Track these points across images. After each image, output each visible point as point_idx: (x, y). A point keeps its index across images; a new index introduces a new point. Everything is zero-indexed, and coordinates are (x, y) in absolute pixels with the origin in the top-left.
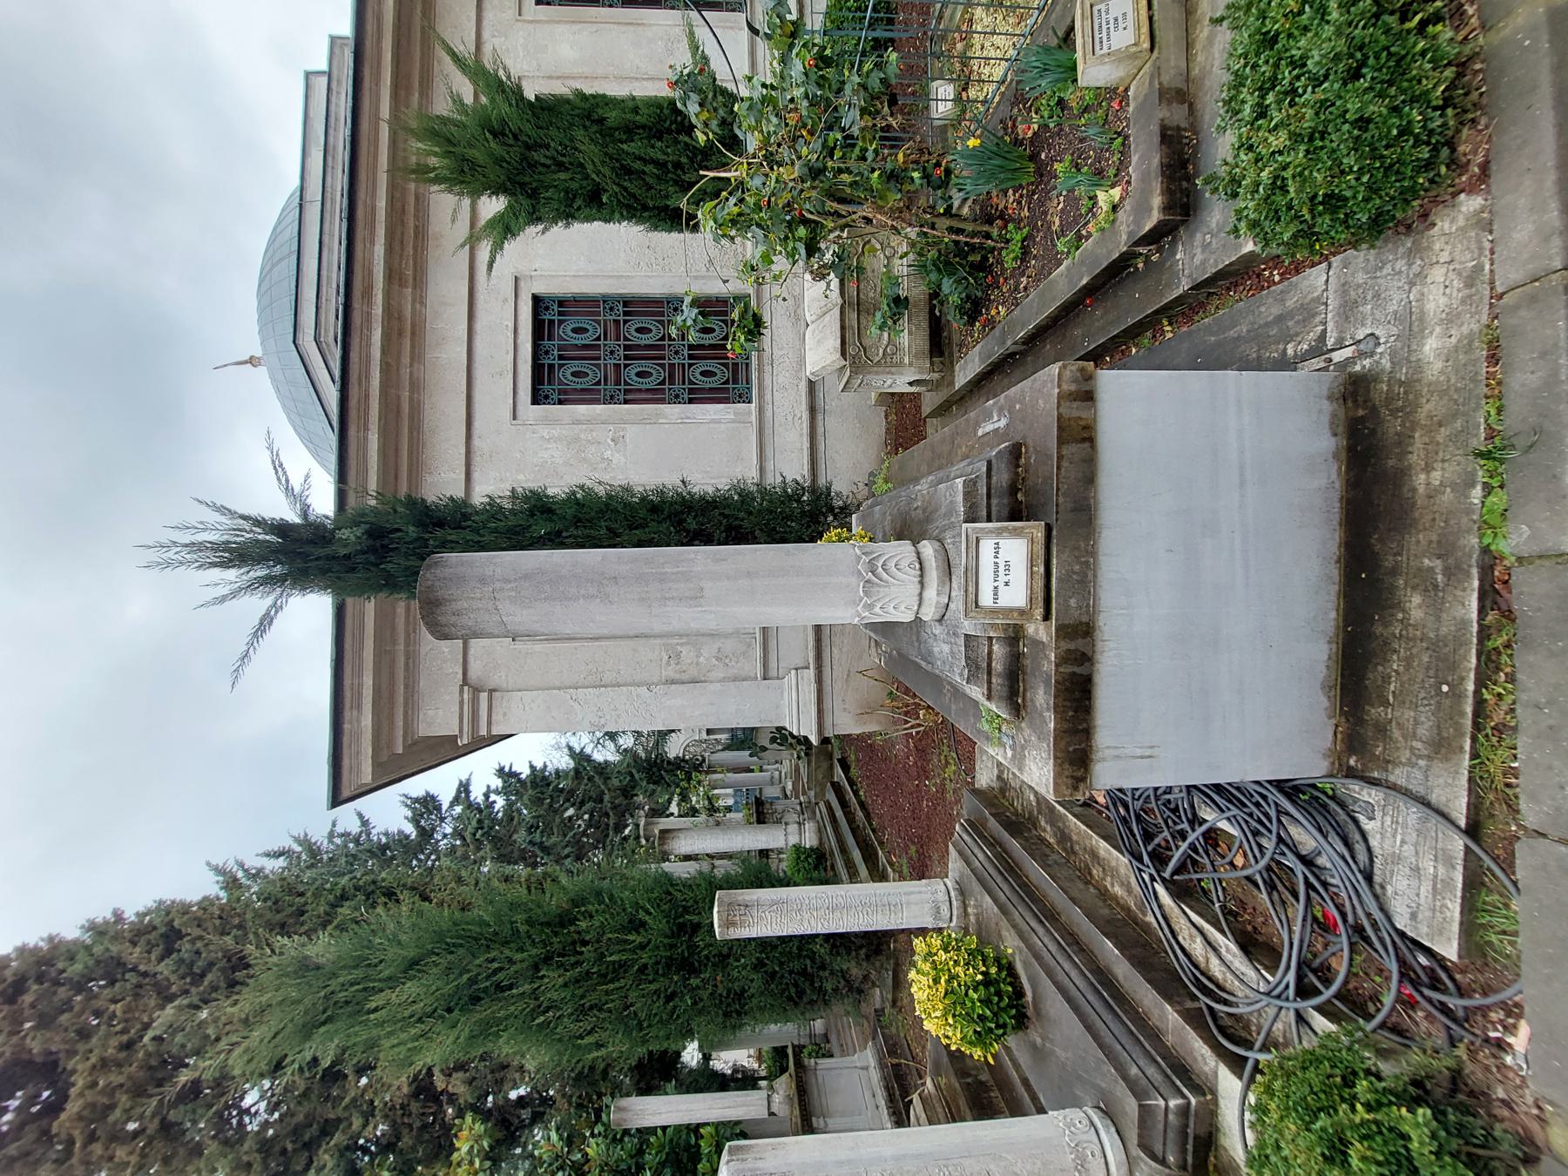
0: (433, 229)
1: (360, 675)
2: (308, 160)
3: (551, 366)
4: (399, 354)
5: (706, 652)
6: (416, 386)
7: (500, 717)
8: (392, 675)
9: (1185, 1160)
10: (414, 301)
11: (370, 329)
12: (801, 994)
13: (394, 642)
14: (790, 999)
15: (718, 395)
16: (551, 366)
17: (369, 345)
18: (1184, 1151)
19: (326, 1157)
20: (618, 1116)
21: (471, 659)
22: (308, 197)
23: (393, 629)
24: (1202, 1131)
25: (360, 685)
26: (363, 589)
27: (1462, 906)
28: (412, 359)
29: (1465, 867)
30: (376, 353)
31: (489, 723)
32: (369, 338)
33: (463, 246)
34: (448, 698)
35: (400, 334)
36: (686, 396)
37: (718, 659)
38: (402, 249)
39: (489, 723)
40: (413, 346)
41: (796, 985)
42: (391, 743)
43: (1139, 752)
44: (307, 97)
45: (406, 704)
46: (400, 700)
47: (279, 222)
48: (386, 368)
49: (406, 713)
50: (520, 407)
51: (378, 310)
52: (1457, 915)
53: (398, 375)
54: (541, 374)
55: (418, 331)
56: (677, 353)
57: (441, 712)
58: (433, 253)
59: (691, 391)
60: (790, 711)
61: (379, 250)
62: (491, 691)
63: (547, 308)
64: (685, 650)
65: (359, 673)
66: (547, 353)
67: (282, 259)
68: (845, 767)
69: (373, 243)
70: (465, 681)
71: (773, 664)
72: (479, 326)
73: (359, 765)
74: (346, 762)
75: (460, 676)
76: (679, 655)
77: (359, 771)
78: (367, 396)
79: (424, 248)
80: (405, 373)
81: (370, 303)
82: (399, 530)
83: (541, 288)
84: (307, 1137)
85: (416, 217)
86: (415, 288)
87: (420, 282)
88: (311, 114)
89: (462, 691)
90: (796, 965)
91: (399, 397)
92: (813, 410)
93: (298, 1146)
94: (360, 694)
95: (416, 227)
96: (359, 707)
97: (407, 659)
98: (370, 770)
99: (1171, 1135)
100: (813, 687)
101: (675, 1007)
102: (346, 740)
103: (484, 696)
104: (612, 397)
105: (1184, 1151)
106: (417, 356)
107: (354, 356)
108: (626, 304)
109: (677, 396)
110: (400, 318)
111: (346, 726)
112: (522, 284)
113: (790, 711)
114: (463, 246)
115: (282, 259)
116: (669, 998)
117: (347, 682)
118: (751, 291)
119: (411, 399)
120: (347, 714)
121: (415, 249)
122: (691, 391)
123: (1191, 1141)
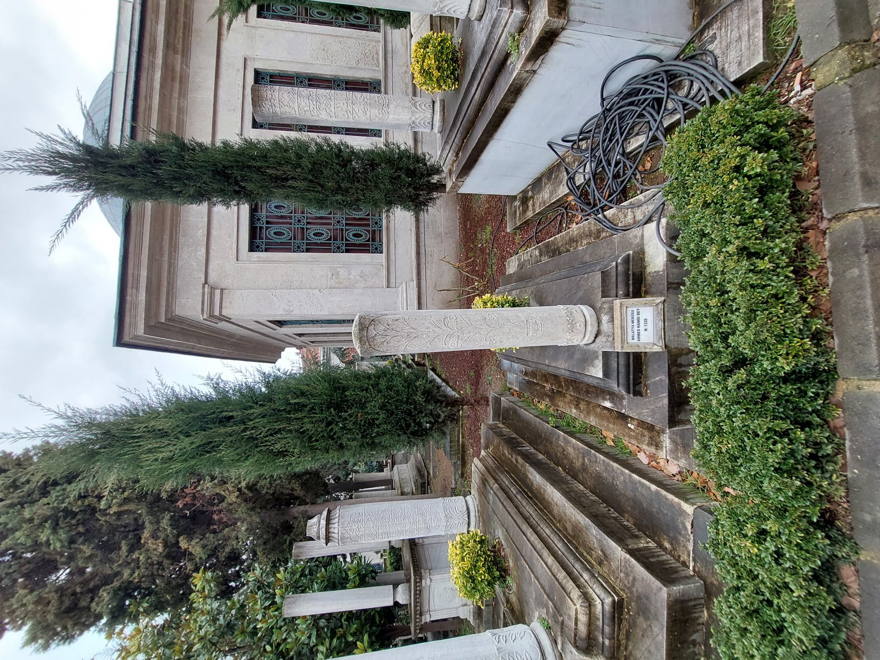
0: (196, 25)
1: (139, 269)
2: (119, 49)
3: (261, 228)
4: (172, 90)
5: (354, 272)
6: (181, 111)
7: (228, 304)
8: (159, 275)
9: (629, 291)
10: (182, 63)
11: (153, 71)
12: (408, 426)
13: (162, 255)
14: (401, 428)
15: (363, 248)
16: (261, 228)
17: (152, 80)
18: (627, 285)
19: (105, 594)
20: (298, 550)
21: (210, 271)
22: (118, 70)
23: (161, 247)
24: (637, 271)
25: (139, 275)
26: (146, 193)
27: (764, 30)
28: (180, 95)
29: (764, 8)
30: (157, 85)
31: (221, 308)
32: (153, 76)
33: (213, 16)
34: (195, 292)
35: (173, 80)
36: (344, 248)
37: (361, 277)
38: (176, 33)
39: (221, 308)
40: (180, 88)
41: (405, 420)
42: (157, 314)
43: (593, 5)
44: (119, 13)
45: (168, 293)
46: (165, 283)
47: (100, 88)
48: (162, 96)
49: (167, 299)
50: (245, 129)
51: (159, 61)
52: (761, 35)
53: (170, 103)
54: (254, 232)
55: (184, 81)
56: (339, 222)
57: (190, 300)
58: (194, 40)
59: (347, 245)
60: (402, 304)
61: (161, 28)
62: (222, 290)
63: (263, 78)
64: (341, 271)
65: (138, 266)
66: (259, 220)
67: (100, 109)
68: (434, 370)
69: (157, 23)
70: (206, 283)
71: (392, 280)
72: (221, 83)
73: (136, 323)
74: (127, 320)
75: (203, 280)
76: (338, 273)
77: (136, 327)
78: (150, 108)
79: (190, 35)
80: (175, 102)
81: (154, 56)
82: (167, 150)
83: (260, 66)
84: (92, 585)
85: (185, 17)
86: (183, 56)
87: (186, 53)
88: (122, 23)
89: (204, 287)
90: (405, 407)
91: (170, 115)
92: (418, 253)
93: (85, 589)
94: (138, 281)
95: (185, 23)
96: (137, 288)
97: (170, 267)
98: (143, 327)
99: (620, 279)
100: (416, 290)
101: (332, 429)
102: (128, 306)
103: (218, 292)
104: (298, 247)
105: (627, 285)
106: (183, 94)
107: (143, 83)
108: (309, 80)
109: (338, 248)
110: (173, 71)
111: (128, 298)
112: (248, 62)
113: (402, 304)
114: (213, 16)
115: (100, 109)
116: (329, 424)
117: (130, 271)
118: (382, 78)
119: (178, 118)
120: (129, 291)
121: (184, 34)
122: (347, 245)
123: (631, 278)
